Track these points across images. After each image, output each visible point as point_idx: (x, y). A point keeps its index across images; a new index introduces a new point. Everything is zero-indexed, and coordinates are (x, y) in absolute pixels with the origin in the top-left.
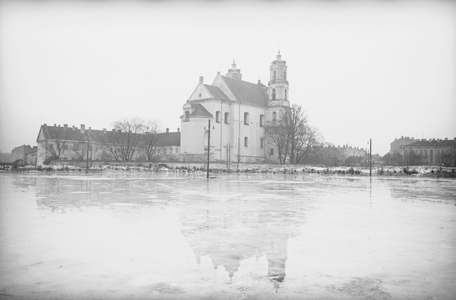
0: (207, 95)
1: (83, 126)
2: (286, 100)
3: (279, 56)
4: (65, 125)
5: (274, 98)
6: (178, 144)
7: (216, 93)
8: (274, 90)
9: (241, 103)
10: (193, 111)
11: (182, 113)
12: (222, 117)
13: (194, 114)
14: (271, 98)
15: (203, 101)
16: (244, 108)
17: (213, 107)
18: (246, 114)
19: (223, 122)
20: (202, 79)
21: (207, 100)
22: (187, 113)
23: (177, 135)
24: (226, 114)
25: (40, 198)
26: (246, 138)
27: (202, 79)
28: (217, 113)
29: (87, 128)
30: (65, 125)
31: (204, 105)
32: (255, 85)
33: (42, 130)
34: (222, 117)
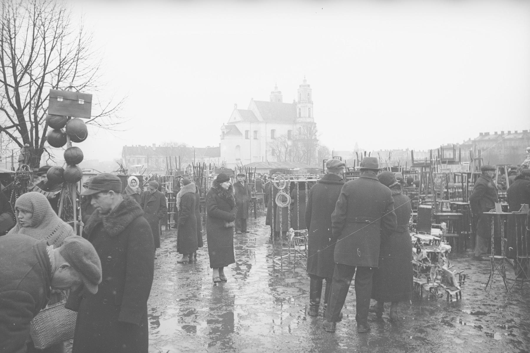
0: (239, 118)
1: (154, 145)
2: (309, 117)
3: (305, 81)
4: (153, 144)
5: (300, 117)
6: (219, 156)
7: (248, 116)
8: (300, 109)
9: (266, 123)
10: (228, 131)
11: (221, 133)
12: (251, 134)
13: (228, 133)
14: (298, 116)
15: (236, 122)
16: (270, 127)
17: (242, 127)
18: (273, 131)
19: (252, 138)
20: (236, 105)
21: (239, 122)
22: (223, 132)
23: (218, 149)
24: (255, 132)
25: (129, 218)
27: (252, 99)
28: (247, 132)
29: (157, 146)
30: (153, 144)
31: (238, 125)
32: (290, 104)
33: (48, 98)
34: (251, 134)
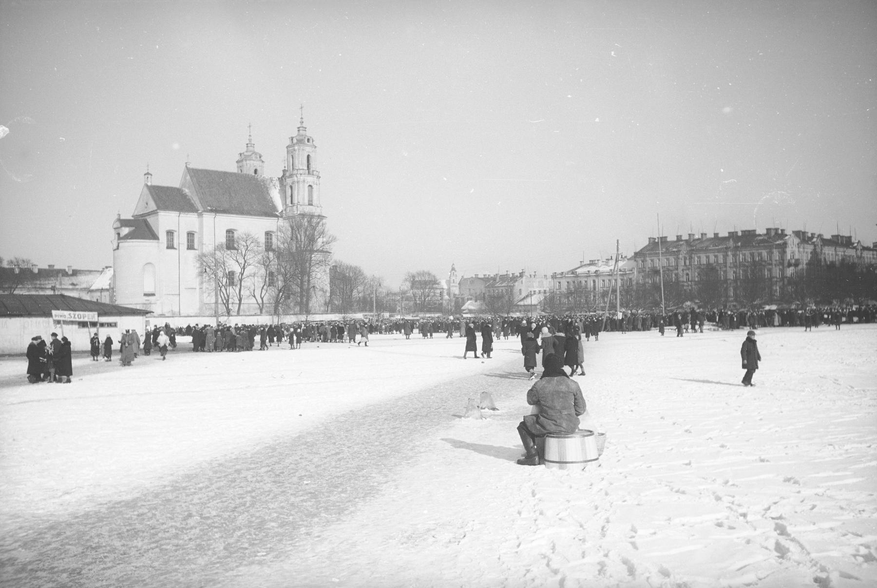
7: (167, 198)
26: (145, 295)
34: (181, 240)
